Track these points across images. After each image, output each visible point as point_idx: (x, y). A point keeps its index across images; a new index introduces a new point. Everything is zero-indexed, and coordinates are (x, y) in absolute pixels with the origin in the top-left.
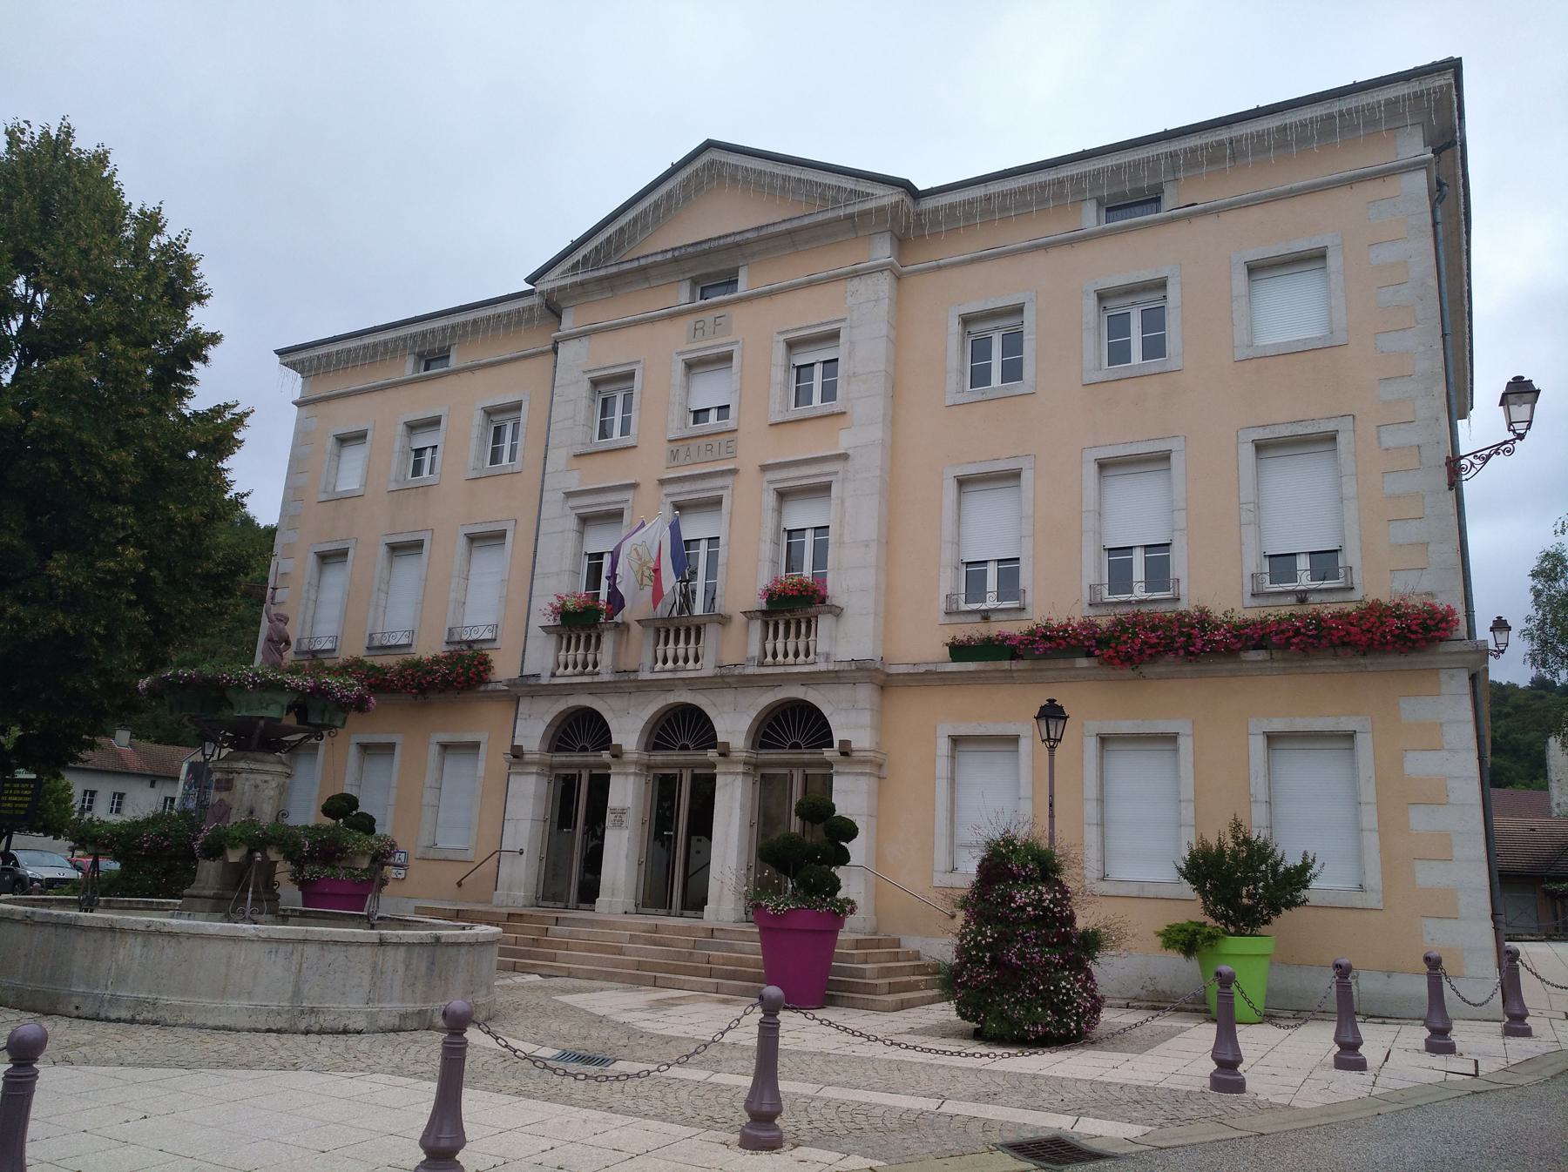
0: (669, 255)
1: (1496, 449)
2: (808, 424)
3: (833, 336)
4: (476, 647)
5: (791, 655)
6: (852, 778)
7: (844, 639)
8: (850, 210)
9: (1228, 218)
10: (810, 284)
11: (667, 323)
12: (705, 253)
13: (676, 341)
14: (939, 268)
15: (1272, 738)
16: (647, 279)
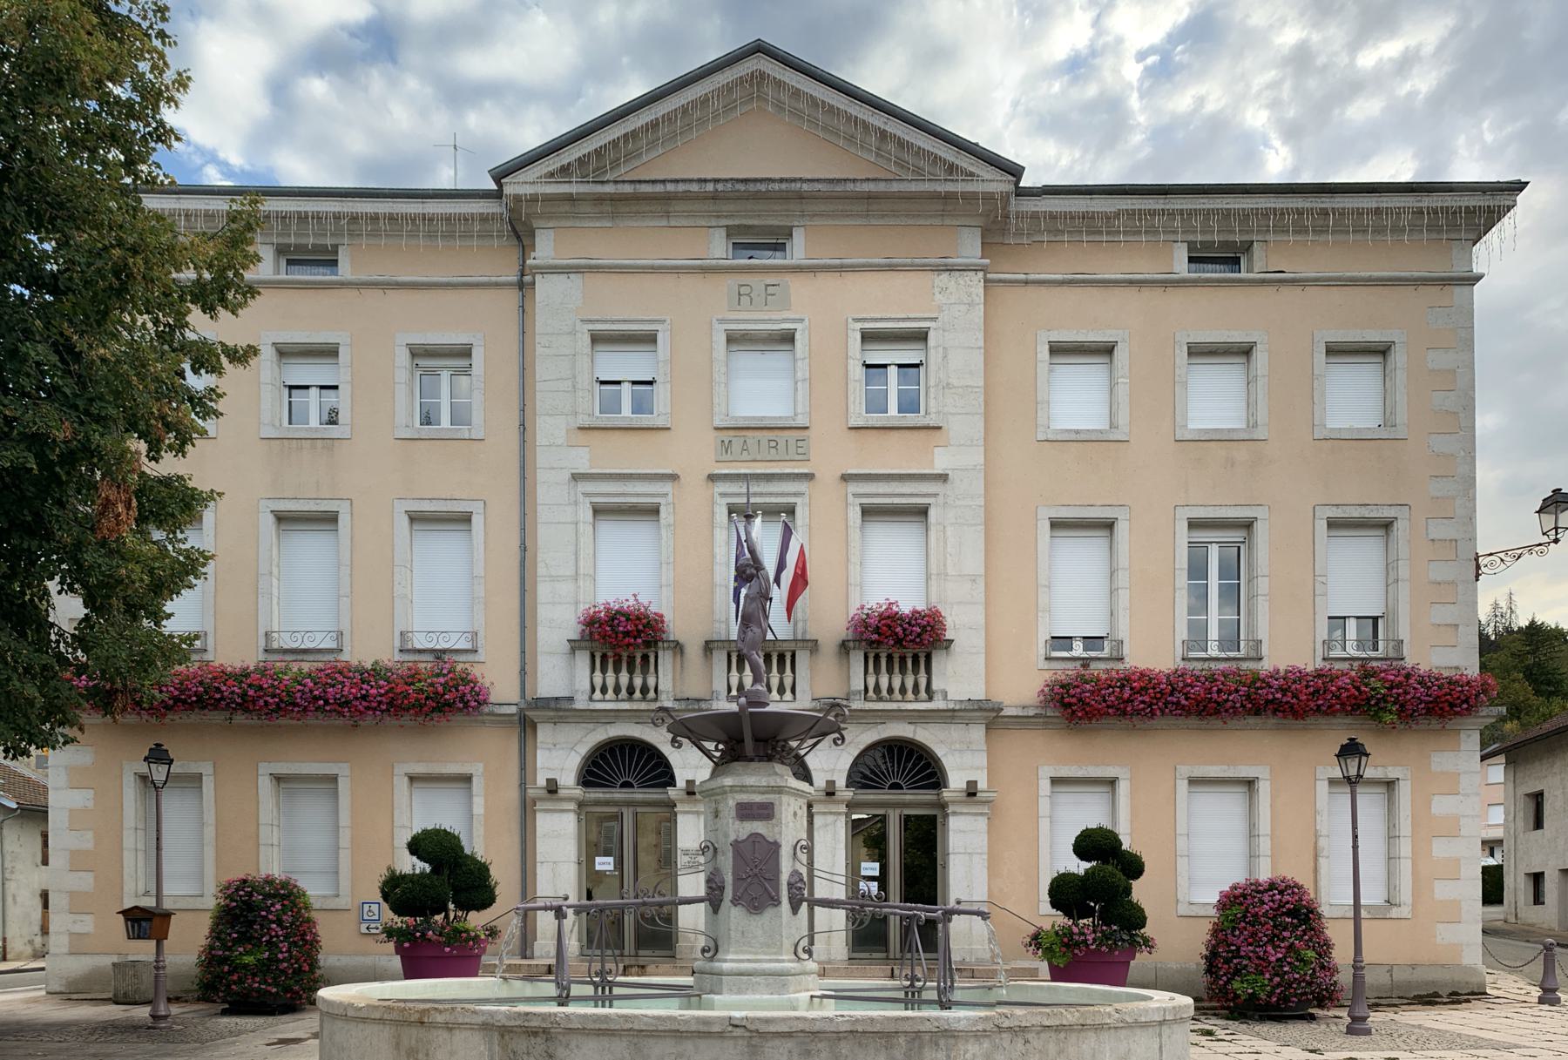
0: (710, 187)
1: (1530, 548)
3: (920, 337)
4: (446, 657)
5: (610, 691)
6: (972, 818)
7: (958, 677)
8: (950, 187)
9: (1312, 291)
12: (757, 197)
15: (1055, 781)
16: (667, 215)
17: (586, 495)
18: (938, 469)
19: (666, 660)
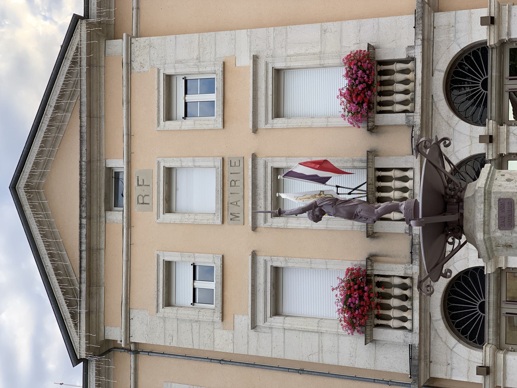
2: (226, 92)
3: (169, 79)
5: (405, 314)
10: (129, 102)
11: (134, 231)
13: (149, 220)
14: (138, 8)
16: (99, 250)
17: (265, 320)
18: (249, 63)
19: (381, 268)
